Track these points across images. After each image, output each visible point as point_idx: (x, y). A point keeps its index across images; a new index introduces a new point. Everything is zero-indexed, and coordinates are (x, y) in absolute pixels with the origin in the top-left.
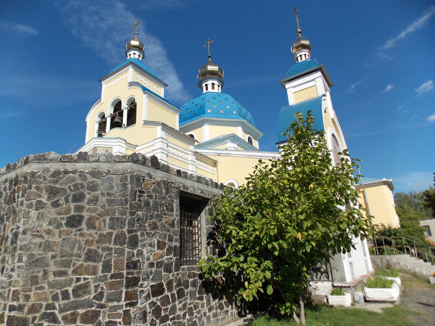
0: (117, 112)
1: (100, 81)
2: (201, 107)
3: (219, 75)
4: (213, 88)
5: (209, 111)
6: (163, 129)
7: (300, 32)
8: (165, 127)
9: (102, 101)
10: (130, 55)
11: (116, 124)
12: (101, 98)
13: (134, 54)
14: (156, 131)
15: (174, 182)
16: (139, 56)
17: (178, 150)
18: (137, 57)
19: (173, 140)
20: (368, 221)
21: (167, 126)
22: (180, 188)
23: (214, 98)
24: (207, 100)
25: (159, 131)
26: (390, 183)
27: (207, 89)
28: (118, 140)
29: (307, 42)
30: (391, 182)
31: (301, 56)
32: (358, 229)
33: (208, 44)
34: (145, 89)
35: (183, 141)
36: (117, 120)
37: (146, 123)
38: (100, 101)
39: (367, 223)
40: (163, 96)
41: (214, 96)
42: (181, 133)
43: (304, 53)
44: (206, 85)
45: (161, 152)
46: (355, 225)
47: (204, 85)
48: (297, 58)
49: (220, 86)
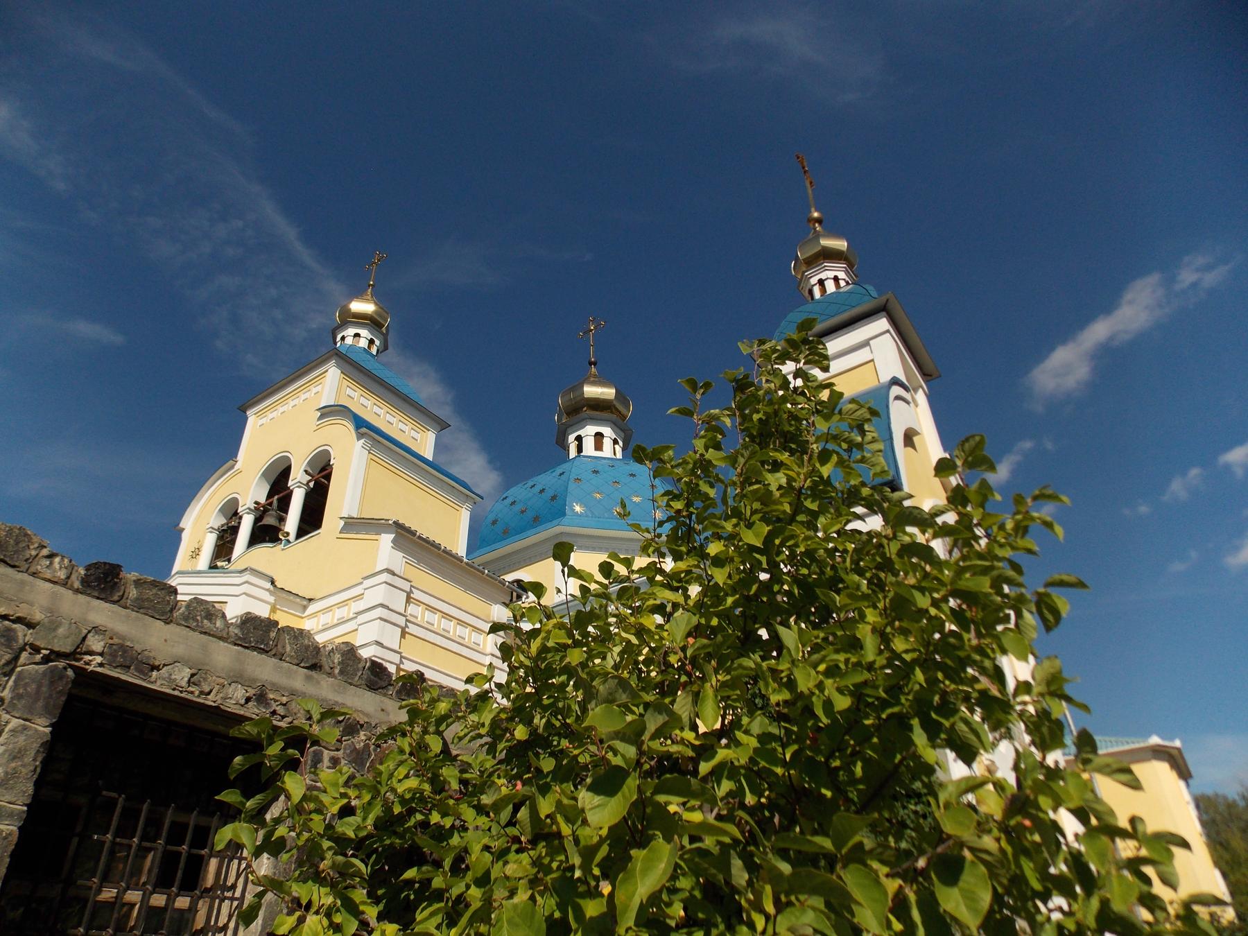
0: (276, 497)
1: (243, 409)
2: (554, 498)
3: (617, 409)
4: (599, 446)
5: (578, 509)
6: (397, 544)
7: (819, 221)
8: (406, 537)
9: (236, 467)
10: (343, 338)
11: (265, 534)
12: (236, 457)
13: (357, 335)
14: (378, 549)
15: (38, 616)
16: (371, 342)
17: (461, 623)
18: (363, 343)
19: (428, 581)
20: (1149, 870)
21: (413, 533)
22: (88, 658)
23: (596, 472)
24: (573, 476)
25: (384, 549)
26: (1175, 752)
27: (580, 449)
28: (247, 577)
29: (841, 244)
30: (1179, 749)
31: (821, 282)
32: (1091, 922)
33: (591, 330)
34: (362, 426)
35: (467, 588)
36: (269, 520)
37: (353, 525)
38: (232, 467)
39: (1147, 881)
40: (429, 454)
41: (597, 468)
42: (483, 573)
43: (831, 274)
44: (579, 439)
45: (381, 619)
46: (1070, 895)
47: (572, 438)
48: (811, 292)
49: (621, 443)
